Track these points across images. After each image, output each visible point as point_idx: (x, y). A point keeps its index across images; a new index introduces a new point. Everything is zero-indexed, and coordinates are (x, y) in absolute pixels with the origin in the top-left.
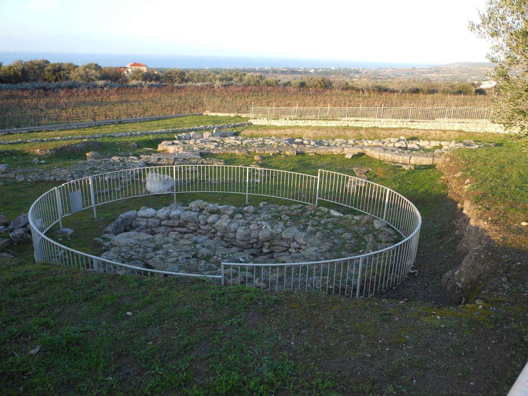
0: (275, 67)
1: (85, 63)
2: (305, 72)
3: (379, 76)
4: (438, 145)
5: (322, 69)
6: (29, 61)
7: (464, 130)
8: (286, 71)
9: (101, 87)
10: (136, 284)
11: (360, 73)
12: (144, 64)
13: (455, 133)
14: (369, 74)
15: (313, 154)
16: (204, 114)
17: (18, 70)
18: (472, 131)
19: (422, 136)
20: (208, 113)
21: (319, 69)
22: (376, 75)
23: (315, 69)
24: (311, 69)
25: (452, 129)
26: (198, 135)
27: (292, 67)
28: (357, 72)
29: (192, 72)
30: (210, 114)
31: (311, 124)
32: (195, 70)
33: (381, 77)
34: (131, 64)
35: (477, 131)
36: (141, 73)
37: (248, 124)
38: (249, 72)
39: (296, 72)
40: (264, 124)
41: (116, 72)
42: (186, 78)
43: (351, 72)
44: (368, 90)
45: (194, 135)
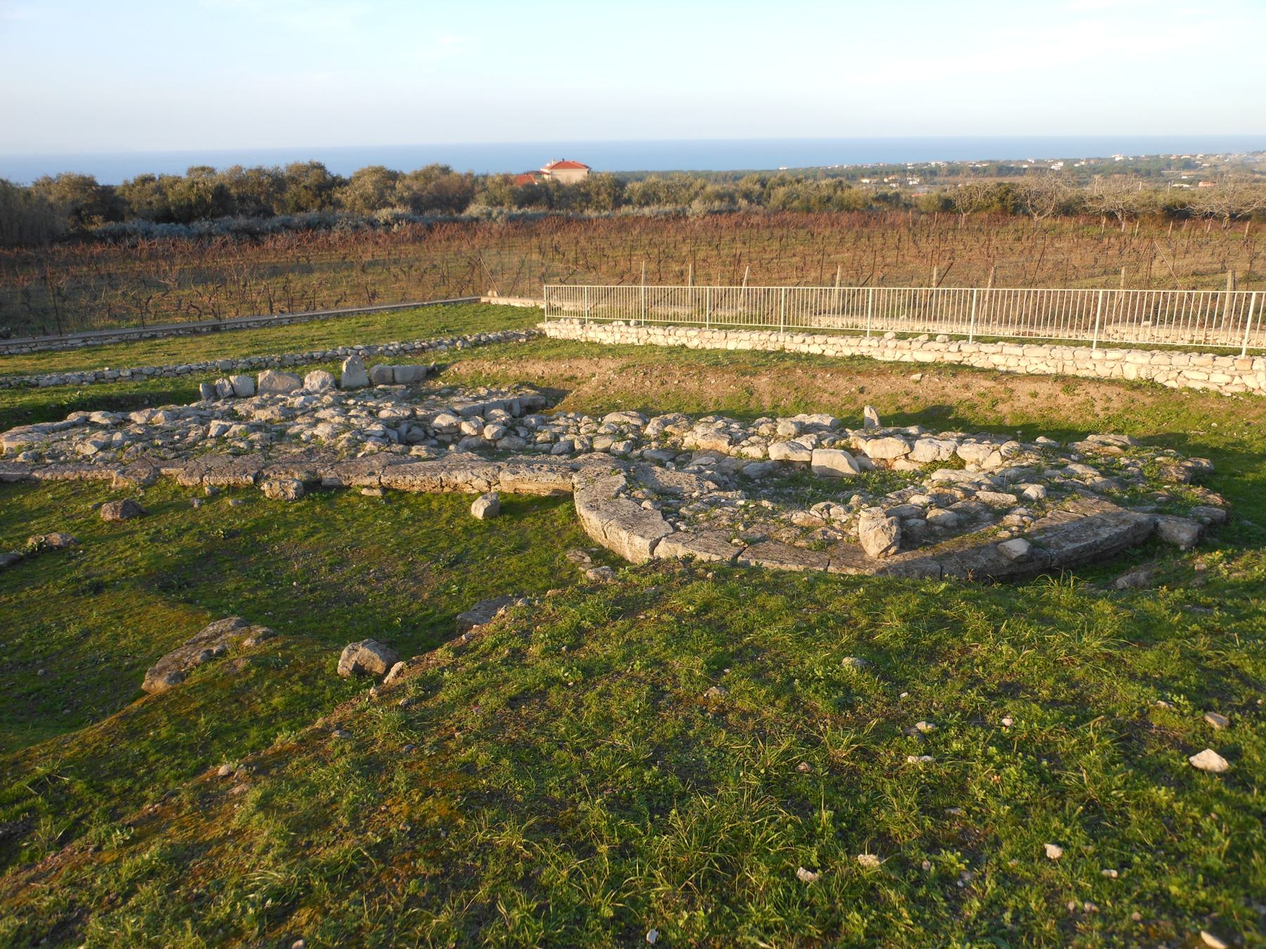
0: (957, 160)
1: (419, 166)
2: (1036, 169)
3: (1254, 172)
4: (945, 456)
5: (1088, 160)
6: (254, 167)
7: (1160, 379)
8: (985, 170)
9: (387, 223)
10: (546, 570)
11: (1196, 166)
12: (583, 163)
13: (1111, 391)
14: (1223, 169)
15: (377, 493)
16: (483, 300)
17: (206, 191)
18: (1191, 385)
19: (977, 400)
20: (494, 298)
21: (1078, 161)
22: (1149, 169)
23: (1065, 161)
24: (1056, 161)
25: (1116, 373)
26: (281, 382)
27: (1001, 158)
28: (1188, 165)
29: (653, 179)
30: (494, 301)
31: (684, 341)
32: (663, 175)
33: (1257, 176)
34: (553, 163)
35: (1213, 388)
36: (508, 187)
37: (529, 335)
38: (887, 174)
39: (1012, 169)
40: (573, 336)
41: (460, 187)
42: (626, 195)
43: (1169, 166)
44: (1132, 216)
45: (270, 379)
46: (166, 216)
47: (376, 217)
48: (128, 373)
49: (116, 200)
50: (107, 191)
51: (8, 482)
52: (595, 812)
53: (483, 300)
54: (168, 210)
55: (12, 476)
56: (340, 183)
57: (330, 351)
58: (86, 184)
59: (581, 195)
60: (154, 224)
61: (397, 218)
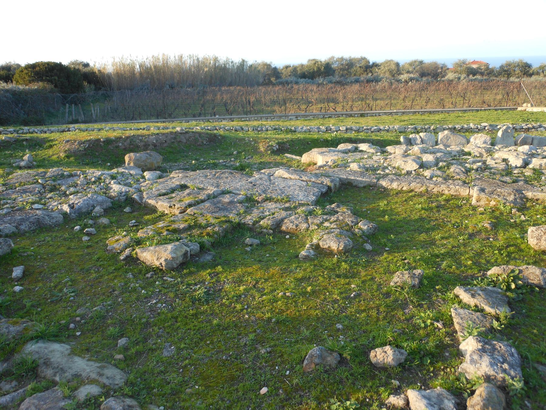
17: (321, 65)
45: (447, 138)
46: (304, 76)
47: (400, 78)
48: (344, 128)
49: (278, 73)
50: (275, 69)
51: (356, 186)
52: (187, 299)
53: (519, 109)
54: (304, 74)
55: (361, 182)
56: (375, 65)
57: (466, 126)
58: (268, 66)
59: (506, 71)
60: (299, 79)
61: (411, 79)
